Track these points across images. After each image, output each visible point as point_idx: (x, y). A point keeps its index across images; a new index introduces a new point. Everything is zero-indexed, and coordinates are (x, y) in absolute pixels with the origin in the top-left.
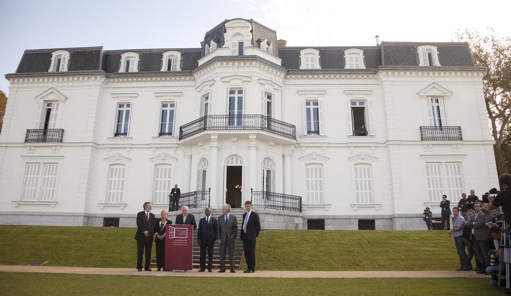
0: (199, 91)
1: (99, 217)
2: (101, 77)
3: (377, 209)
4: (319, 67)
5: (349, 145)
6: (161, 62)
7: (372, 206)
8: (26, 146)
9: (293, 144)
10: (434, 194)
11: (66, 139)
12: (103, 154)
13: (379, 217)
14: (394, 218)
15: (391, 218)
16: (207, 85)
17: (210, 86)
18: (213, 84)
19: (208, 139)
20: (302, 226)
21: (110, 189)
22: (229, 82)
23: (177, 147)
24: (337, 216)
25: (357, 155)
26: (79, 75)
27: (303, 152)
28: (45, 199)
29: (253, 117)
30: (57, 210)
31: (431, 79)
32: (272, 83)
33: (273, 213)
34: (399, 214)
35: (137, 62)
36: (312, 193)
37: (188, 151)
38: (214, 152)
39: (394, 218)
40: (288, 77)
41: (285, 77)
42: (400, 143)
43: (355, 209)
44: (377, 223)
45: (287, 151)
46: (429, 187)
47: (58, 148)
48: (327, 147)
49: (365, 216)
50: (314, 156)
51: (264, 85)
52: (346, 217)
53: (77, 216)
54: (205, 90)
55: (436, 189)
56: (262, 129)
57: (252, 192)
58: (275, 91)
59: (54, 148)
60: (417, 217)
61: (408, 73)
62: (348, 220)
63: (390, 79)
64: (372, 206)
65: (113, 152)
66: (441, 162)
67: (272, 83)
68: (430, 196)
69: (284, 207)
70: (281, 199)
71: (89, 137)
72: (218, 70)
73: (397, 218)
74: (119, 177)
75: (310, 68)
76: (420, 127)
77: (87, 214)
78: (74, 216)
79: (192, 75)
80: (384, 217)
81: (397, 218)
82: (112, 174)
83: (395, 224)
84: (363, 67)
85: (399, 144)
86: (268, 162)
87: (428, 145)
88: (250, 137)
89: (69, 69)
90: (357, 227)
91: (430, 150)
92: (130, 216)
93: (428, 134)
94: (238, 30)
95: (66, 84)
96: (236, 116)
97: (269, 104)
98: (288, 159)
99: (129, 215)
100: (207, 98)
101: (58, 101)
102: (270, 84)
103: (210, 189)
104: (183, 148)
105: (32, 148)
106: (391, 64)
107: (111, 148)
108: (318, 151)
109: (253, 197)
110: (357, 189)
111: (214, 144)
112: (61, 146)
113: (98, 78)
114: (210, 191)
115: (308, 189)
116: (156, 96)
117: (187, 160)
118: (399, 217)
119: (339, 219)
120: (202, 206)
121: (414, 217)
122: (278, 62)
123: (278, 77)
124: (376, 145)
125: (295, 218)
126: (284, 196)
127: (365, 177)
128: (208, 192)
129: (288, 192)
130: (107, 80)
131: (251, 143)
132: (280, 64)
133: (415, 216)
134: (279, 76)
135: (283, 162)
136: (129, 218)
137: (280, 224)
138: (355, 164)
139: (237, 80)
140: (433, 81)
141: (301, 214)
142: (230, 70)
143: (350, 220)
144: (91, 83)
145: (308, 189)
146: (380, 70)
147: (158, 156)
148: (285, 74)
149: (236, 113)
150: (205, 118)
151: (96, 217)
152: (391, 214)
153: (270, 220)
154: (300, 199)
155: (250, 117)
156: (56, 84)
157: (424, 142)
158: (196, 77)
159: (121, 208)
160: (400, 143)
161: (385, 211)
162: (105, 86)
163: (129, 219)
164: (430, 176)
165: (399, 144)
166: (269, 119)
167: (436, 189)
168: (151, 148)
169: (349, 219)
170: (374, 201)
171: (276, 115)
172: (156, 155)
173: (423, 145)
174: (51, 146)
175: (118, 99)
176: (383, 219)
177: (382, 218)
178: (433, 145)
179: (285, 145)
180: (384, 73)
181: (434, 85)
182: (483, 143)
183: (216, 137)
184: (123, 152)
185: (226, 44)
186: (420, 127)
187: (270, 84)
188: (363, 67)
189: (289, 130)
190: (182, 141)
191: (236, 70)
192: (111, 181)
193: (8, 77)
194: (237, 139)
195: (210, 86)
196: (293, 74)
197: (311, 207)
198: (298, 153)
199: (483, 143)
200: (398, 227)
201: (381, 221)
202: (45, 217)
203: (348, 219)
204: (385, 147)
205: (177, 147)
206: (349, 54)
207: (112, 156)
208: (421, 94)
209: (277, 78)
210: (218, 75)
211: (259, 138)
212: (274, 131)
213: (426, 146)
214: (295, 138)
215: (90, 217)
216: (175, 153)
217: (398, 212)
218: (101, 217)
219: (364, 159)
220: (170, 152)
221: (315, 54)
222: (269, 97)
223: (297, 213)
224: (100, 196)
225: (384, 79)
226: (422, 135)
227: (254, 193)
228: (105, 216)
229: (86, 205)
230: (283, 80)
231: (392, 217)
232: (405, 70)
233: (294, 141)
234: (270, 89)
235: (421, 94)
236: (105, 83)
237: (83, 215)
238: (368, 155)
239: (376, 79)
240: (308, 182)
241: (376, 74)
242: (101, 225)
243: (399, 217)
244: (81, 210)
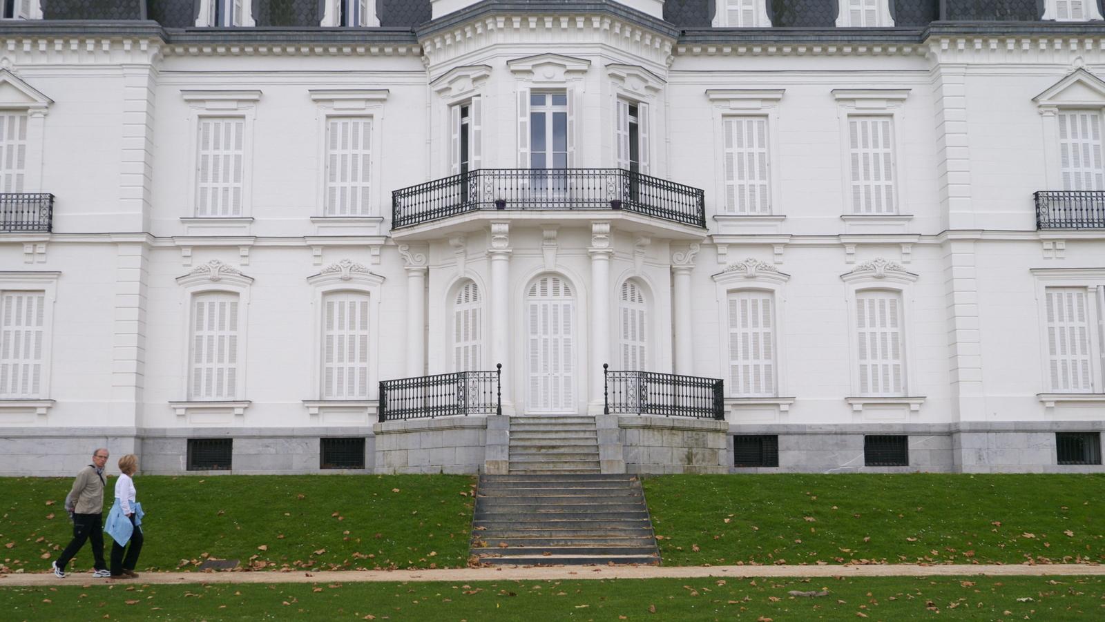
0: (440, 92)
1: (172, 438)
2: (152, 42)
3: (913, 407)
4: (764, 22)
7: (902, 402)
9: (698, 240)
10: (1065, 371)
11: (65, 220)
13: (919, 429)
14: (959, 431)
15: (951, 433)
16: (468, 76)
17: (475, 80)
18: (486, 76)
19: (482, 232)
20: (724, 460)
21: (199, 360)
22: (529, 72)
23: (382, 247)
24: (810, 427)
25: (864, 268)
26: (83, 34)
27: (721, 259)
28: (14, 390)
29: (600, 175)
30: (54, 422)
31: (1073, 58)
32: (642, 72)
33: (659, 424)
34: (970, 423)
36: (746, 367)
37: (417, 261)
38: (499, 265)
39: (959, 431)
40: (682, 50)
41: (675, 51)
42: (979, 237)
43: (856, 407)
44: (913, 443)
45: (682, 259)
46: (1053, 351)
47: (41, 249)
48: (786, 245)
49: (883, 426)
50: (751, 271)
51: (622, 79)
52: (834, 429)
53: (116, 437)
54: (461, 88)
55: (1069, 357)
56: (616, 205)
57: (606, 372)
59: (29, 249)
60: (1016, 431)
61: (1011, 44)
62: (839, 436)
63: (960, 59)
64: (902, 402)
65: (203, 259)
66: (1085, 287)
67: (642, 72)
68: (1054, 375)
69: (675, 408)
70: (668, 389)
71: (130, 218)
72: (499, 38)
73: (965, 431)
74: (222, 327)
75: (741, 24)
76: (1036, 194)
77: (145, 430)
78: (107, 437)
79: (415, 41)
80: (933, 429)
81: (965, 431)
82: (200, 320)
83: (960, 448)
84: (887, 22)
86: (633, 288)
87: (1054, 241)
89: (48, 14)
90: (862, 455)
91: (1059, 254)
92: (262, 434)
93: (1055, 213)
96: (550, 172)
97: (634, 129)
98: (683, 280)
99: (260, 429)
100: (465, 112)
101: (25, 109)
102: (637, 76)
103: (499, 366)
104: (401, 250)
106: (965, 12)
108: (763, 257)
110: (862, 355)
111: (500, 246)
112: (49, 243)
113: (144, 45)
114: (499, 372)
115: (734, 356)
116: (315, 101)
117: (415, 282)
118: (970, 431)
119: (816, 434)
120: (482, 410)
121: (1008, 431)
124: (914, 240)
125: (710, 436)
126: (675, 380)
127: (751, 145)
128: (495, 375)
129: (685, 370)
130: (167, 50)
131: (596, 244)
132: (659, 15)
133: (1013, 428)
135: (673, 286)
136: (261, 437)
137: (675, 451)
138: (858, 291)
140: (1079, 64)
141: (719, 424)
142: (531, 38)
143: (844, 437)
144: (120, 58)
145: (734, 356)
146: (935, 33)
147: (331, 270)
148: (675, 41)
149: (549, 164)
150: (465, 177)
151: (165, 438)
152: (950, 421)
153: (651, 444)
154: (718, 386)
155: (594, 175)
156: (12, 58)
157: (1044, 235)
158: (427, 50)
159: (40, 411)
160: (979, 237)
161: (933, 415)
162: (160, 67)
163: (260, 442)
164: (1057, 324)
166: (633, 176)
167: (1069, 357)
168: (310, 247)
169: (842, 434)
170: (906, 388)
171: (651, 166)
172: (326, 266)
173: (1040, 241)
174: (21, 244)
175: (202, 105)
176: (929, 434)
177: (926, 432)
178: (1068, 241)
179: (676, 243)
180: (945, 44)
183: (506, 228)
184: (231, 260)
186: (1036, 194)
187: (637, 76)
188: (887, 22)
189: (687, 204)
191: (547, 38)
192: (199, 338)
194: (558, 231)
195: (475, 80)
196: (696, 41)
197: (746, 404)
198: (708, 262)
200: (970, 464)
201: (921, 440)
202: (20, 441)
203: (840, 433)
204: (941, 246)
205: (382, 247)
207: (200, 271)
209: (652, 57)
210: (499, 51)
211: (619, 232)
212: (646, 206)
213: (1049, 246)
214: (702, 223)
215: (148, 438)
216: (376, 260)
217: (970, 415)
218: (314, 437)
219: (880, 277)
220: (364, 260)
222: (633, 111)
223: (709, 422)
225: (942, 59)
226: (1038, 215)
227: (610, 375)
228: (324, 434)
229: (137, 404)
230: (669, 57)
231: (953, 429)
232: (1003, 33)
233: (701, 233)
234: (634, 87)
235: (1043, 101)
236: (162, 57)
237: (135, 433)
239: (923, 55)
240: (734, 336)
241: (921, 41)
243: (970, 431)
244: (127, 422)
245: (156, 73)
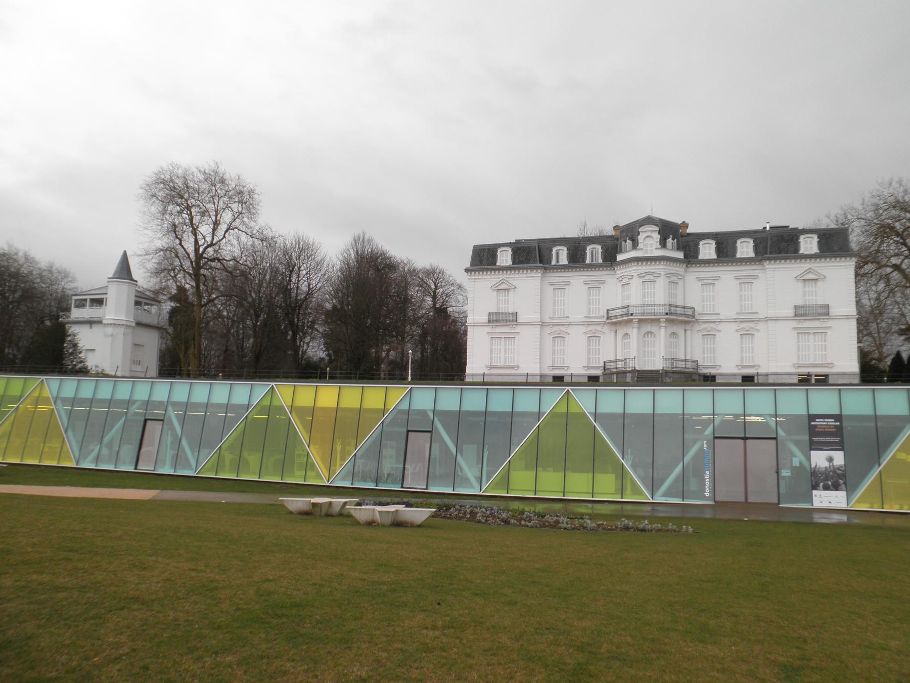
5: (737, 320)
6: (585, 254)
8: (796, 320)
12: (548, 330)
22: (644, 277)
30: (519, 372)
32: (676, 275)
35: (566, 254)
38: (635, 330)
40: (689, 266)
41: (687, 266)
51: (670, 277)
58: (678, 280)
65: (555, 329)
70: (684, 363)
81: (876, 424)
85: (474, 326)
88: (661, 320)
94: (649, 234)
95: (513, 276)
105: (514, 326)
107: (553, 325)
109: (664, 361)
112: (516, 325)
115: (704, 353)
117: (613, 334)
119: (726, 375)
122: (680, 255)
123: (680, 269)
129: (688, 358)
131: (662, 324)
134: (682, 267)
139: (649, 276)
145: (704, 353)
151: (546, 376)
154: (697, 361)
165: (474, 326)
168: (584, 324)
172: (588, 330)
174: (819, 319)
181: (809, 271)
182: (847, 317)
185: (640, 246)
189: (689, 312)
190: (608, 321)
193: (467, 270)
199: (847, 317)
203: (735, 375)
206: (741, 243)
208: (798, 278)
209: (680, 269)
218: (551, 376)
221: (712, 244)
224: (548, 362)
225: (767, 267)
238: (752, 328)
242: (551, 381)
244: (538, 372)
245: (543, 277)
